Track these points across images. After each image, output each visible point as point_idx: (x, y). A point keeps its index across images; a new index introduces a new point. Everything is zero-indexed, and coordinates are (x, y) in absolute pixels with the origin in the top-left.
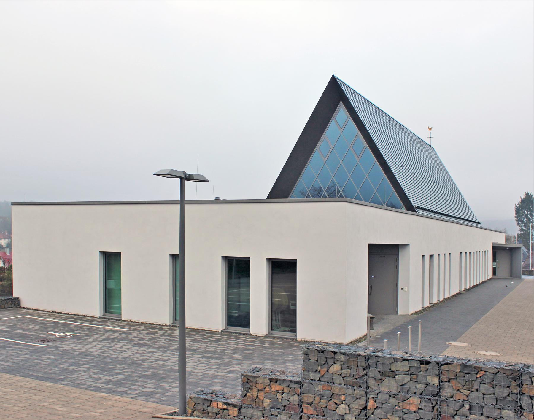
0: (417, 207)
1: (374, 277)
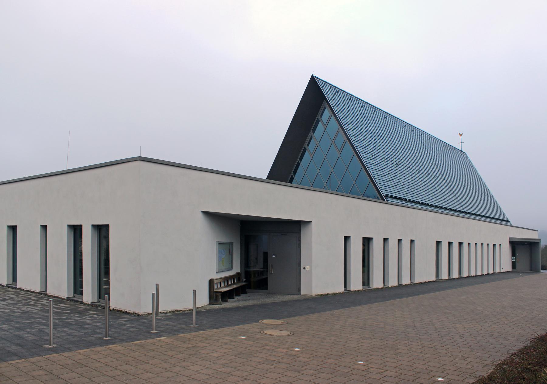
0: (387, 196)
1: (276, 255)
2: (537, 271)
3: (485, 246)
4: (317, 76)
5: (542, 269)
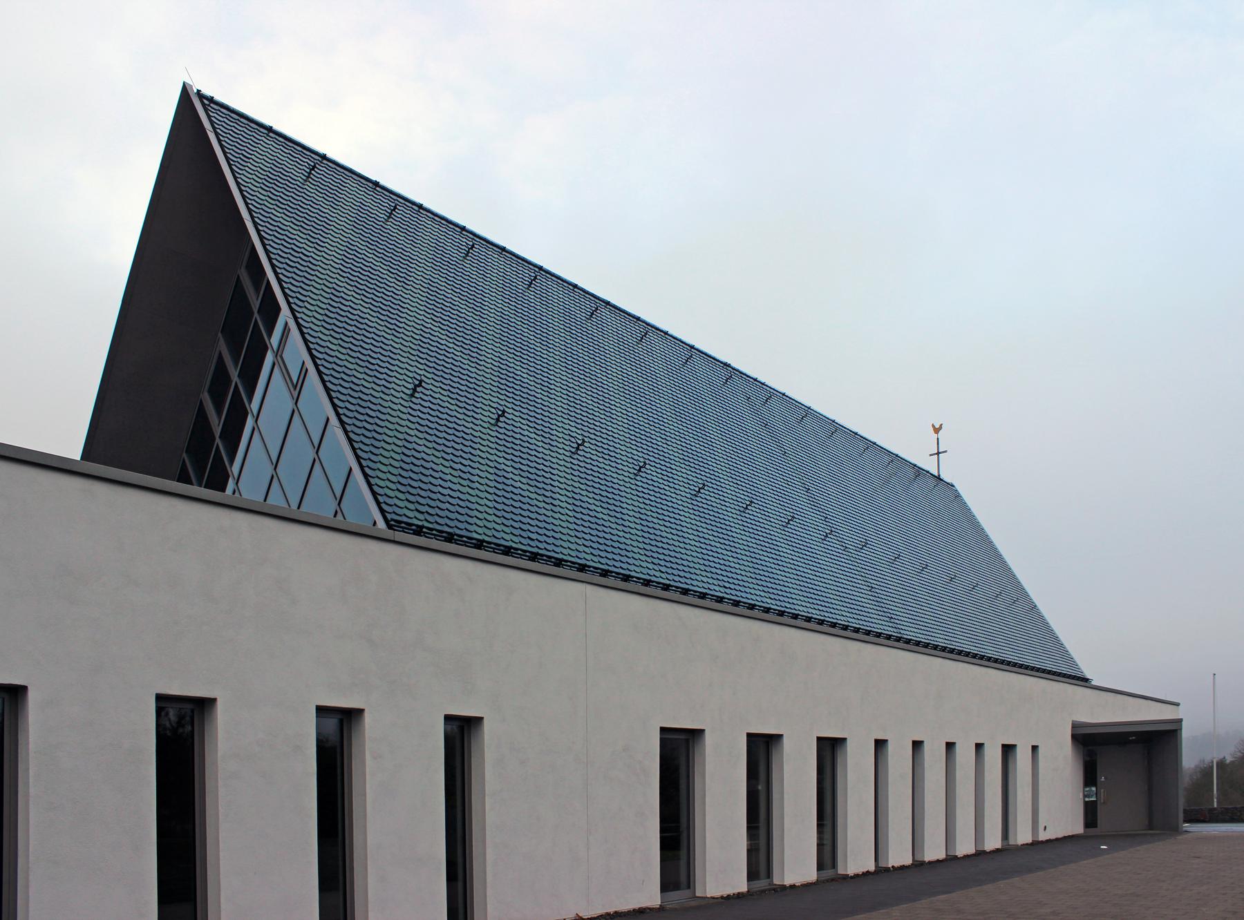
2: (1175, 830)
3: (965, 755)
4: (207, 92)
5: (1185, 821)
